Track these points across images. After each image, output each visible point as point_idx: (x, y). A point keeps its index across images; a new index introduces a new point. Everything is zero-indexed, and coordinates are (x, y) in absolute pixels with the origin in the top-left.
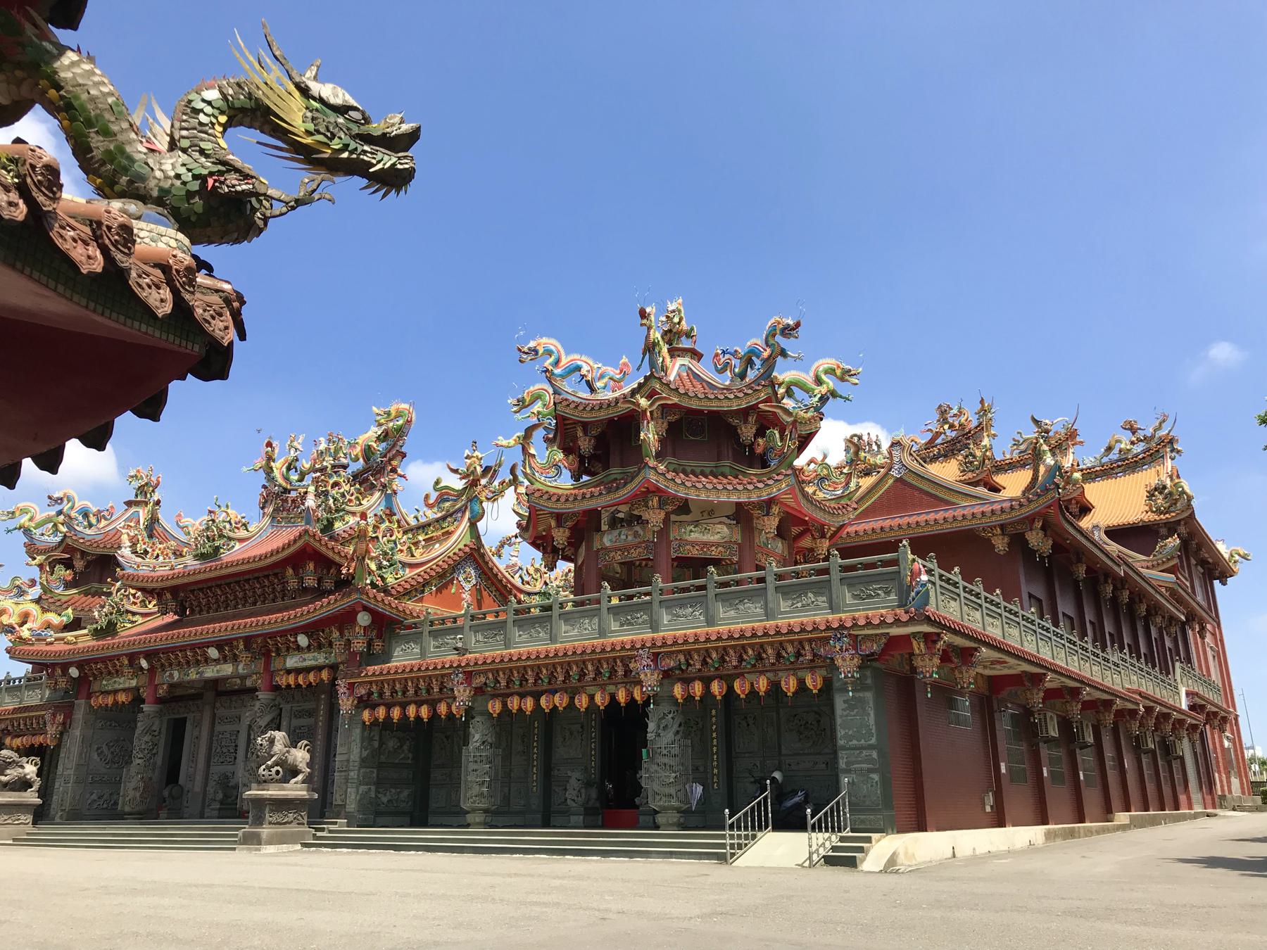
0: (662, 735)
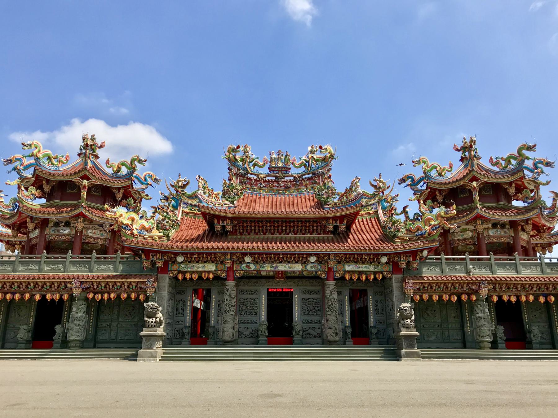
0: (79, 312)
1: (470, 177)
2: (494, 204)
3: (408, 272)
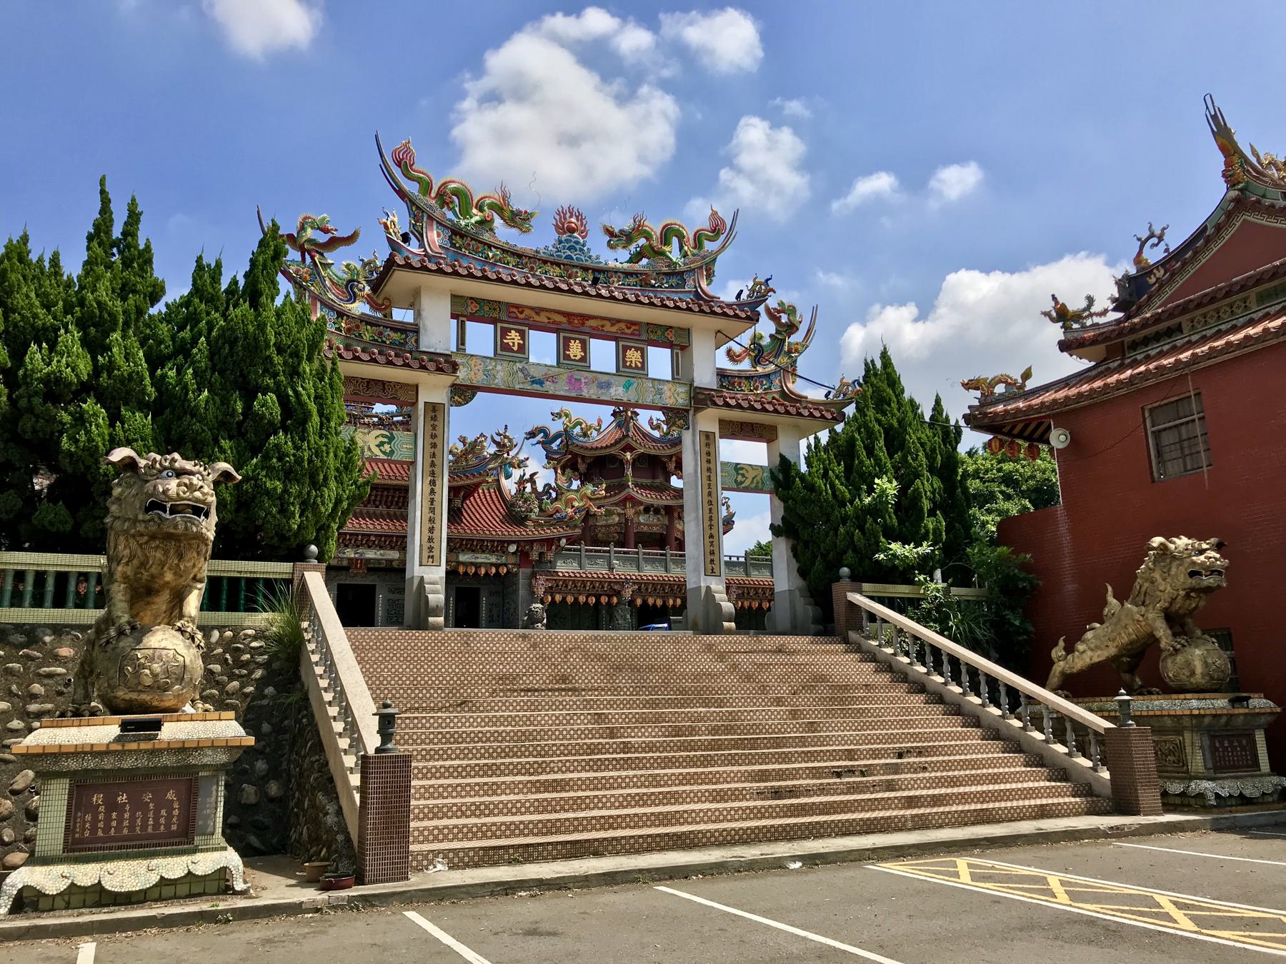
1: (623, 443)
2: (648, 481)
3: (541, 566)
